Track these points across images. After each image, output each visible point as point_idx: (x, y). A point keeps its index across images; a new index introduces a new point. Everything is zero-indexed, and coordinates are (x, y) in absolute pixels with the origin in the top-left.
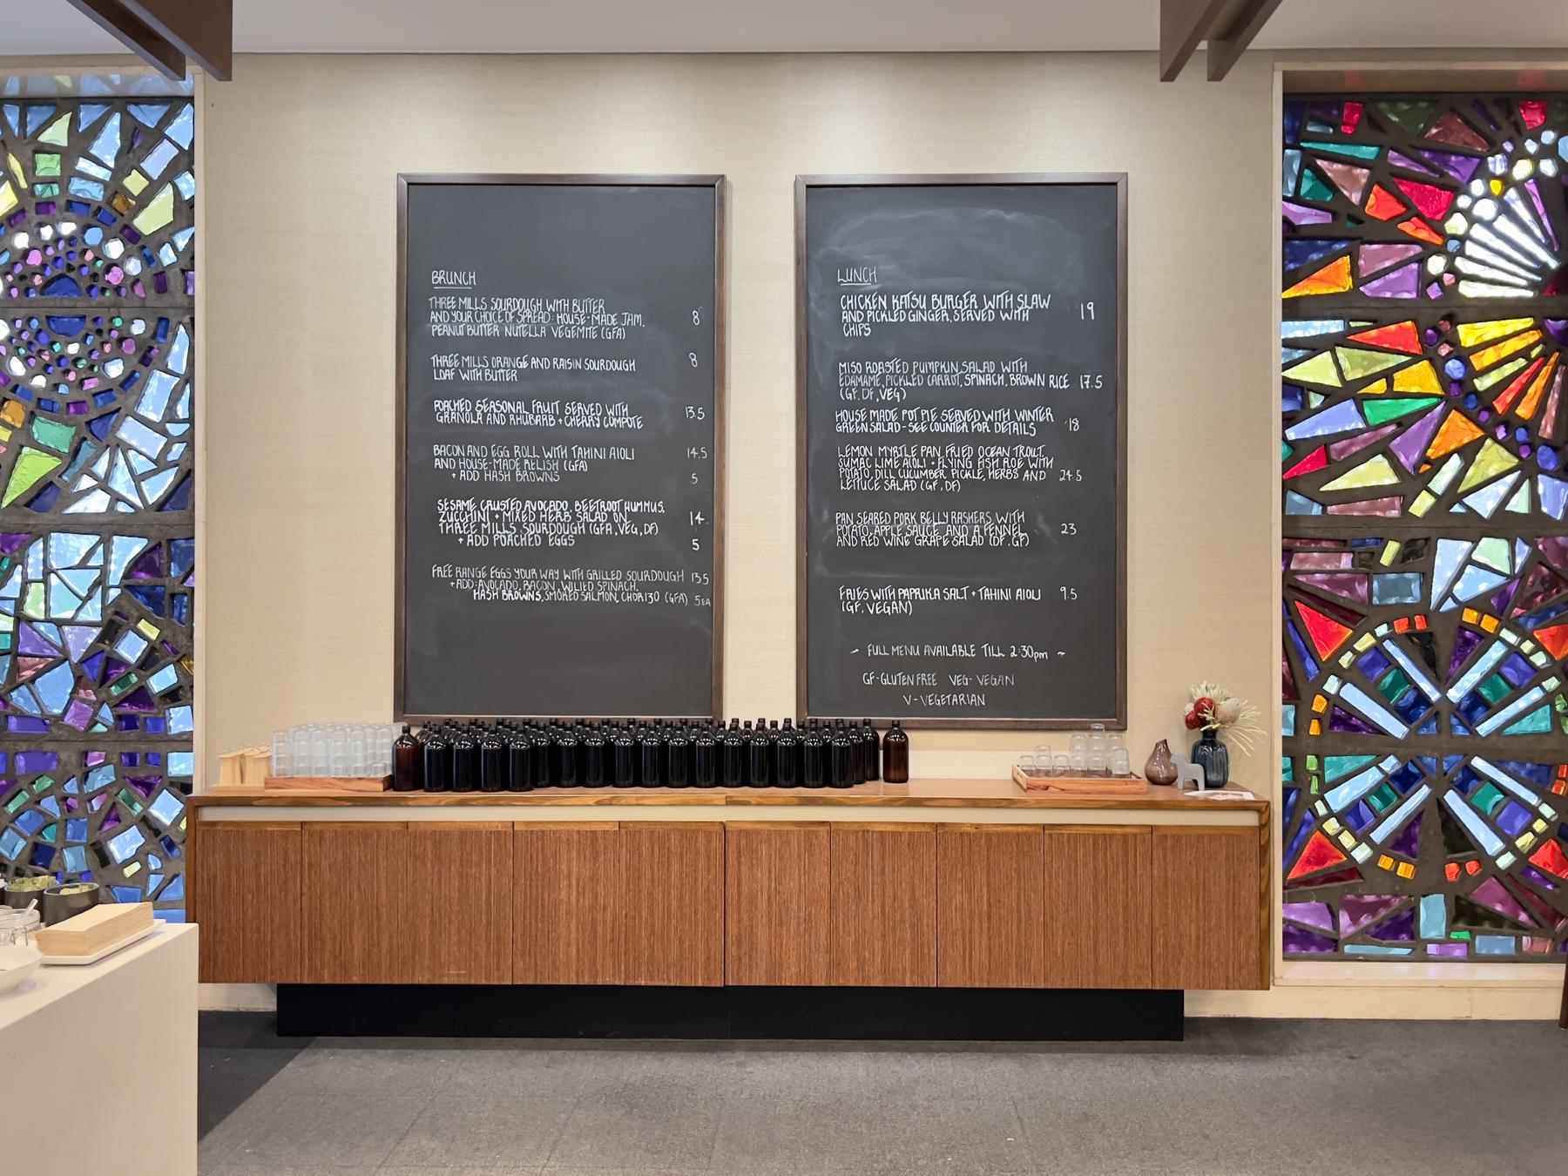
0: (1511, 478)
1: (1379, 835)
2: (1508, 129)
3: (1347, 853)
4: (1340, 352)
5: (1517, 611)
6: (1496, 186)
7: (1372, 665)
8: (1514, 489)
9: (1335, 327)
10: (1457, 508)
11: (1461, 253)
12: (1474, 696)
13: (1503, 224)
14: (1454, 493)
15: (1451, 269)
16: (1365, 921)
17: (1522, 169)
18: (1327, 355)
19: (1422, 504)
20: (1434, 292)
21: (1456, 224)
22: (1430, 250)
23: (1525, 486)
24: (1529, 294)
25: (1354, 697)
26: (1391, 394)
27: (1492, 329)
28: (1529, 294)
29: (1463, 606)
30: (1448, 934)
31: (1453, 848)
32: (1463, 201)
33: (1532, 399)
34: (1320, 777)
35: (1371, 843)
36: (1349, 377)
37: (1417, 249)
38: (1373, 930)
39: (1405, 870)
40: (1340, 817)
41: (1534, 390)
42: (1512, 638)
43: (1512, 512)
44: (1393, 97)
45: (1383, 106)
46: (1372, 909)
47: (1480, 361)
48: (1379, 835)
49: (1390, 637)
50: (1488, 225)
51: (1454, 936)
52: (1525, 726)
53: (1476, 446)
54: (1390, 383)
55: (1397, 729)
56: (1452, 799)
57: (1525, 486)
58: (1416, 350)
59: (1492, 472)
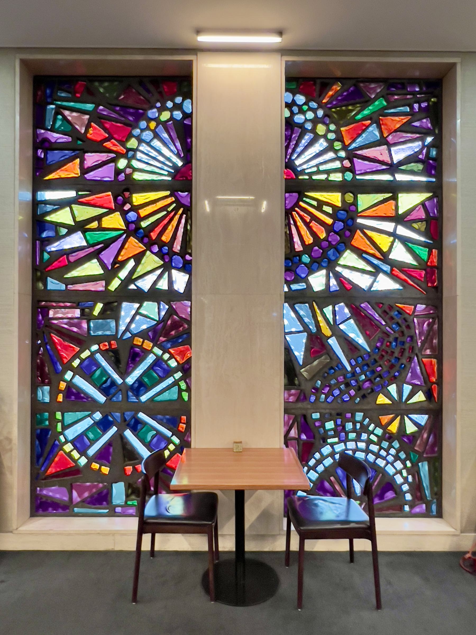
0: (159, 272)
1: (92, 451)
2: (157, 96)
3: (75, 461)
4: (74, 207)
5: (162, 339)
6: (153, 125)
7: (89, 367)
8: (160, 277)
9: (72, 194)
10: (132, 287)
11: (134, 157)
12: (139, 381)
13: (156, 143)
14: (130, 279)
15: (129, 166)
16: (86, 495)
17: (165, 116)
18: (68, 209)
19: (115, 284)
20: (122, 177)
21: (132, 143)
22: (119, 155)
23: (166, 275)
24: (170, 179)
25: (80, 382)
26: (100, 229)
27: (152, 196)
28: (170, 179)
29: (134, 336)
30: (126, 502)
31: (130, 459)
32: (136, 132)
33: (170, 232)
34: (62, 421)
35: (87, 457)
36: (78, 219)
37: (113, 155)
38: (89, 499)
39: (105, 470)
40: (73, 442)
41: (171, 229)
42: (158, 351)
43: (158, 289)
44: (101, 79)
45: (97, 84)
46: (89, 488)
47: (143, 212)
48: (92, 451)
49: (99, 351)
50: (148, 144)
51: (129, 503)
52: (166, 396)
53: (142, 254)
54: (100, 223)
55: (101, 398)
56: (128, 434)
57: (166, 275)
58: (113, 205)
59: (149, 269)
